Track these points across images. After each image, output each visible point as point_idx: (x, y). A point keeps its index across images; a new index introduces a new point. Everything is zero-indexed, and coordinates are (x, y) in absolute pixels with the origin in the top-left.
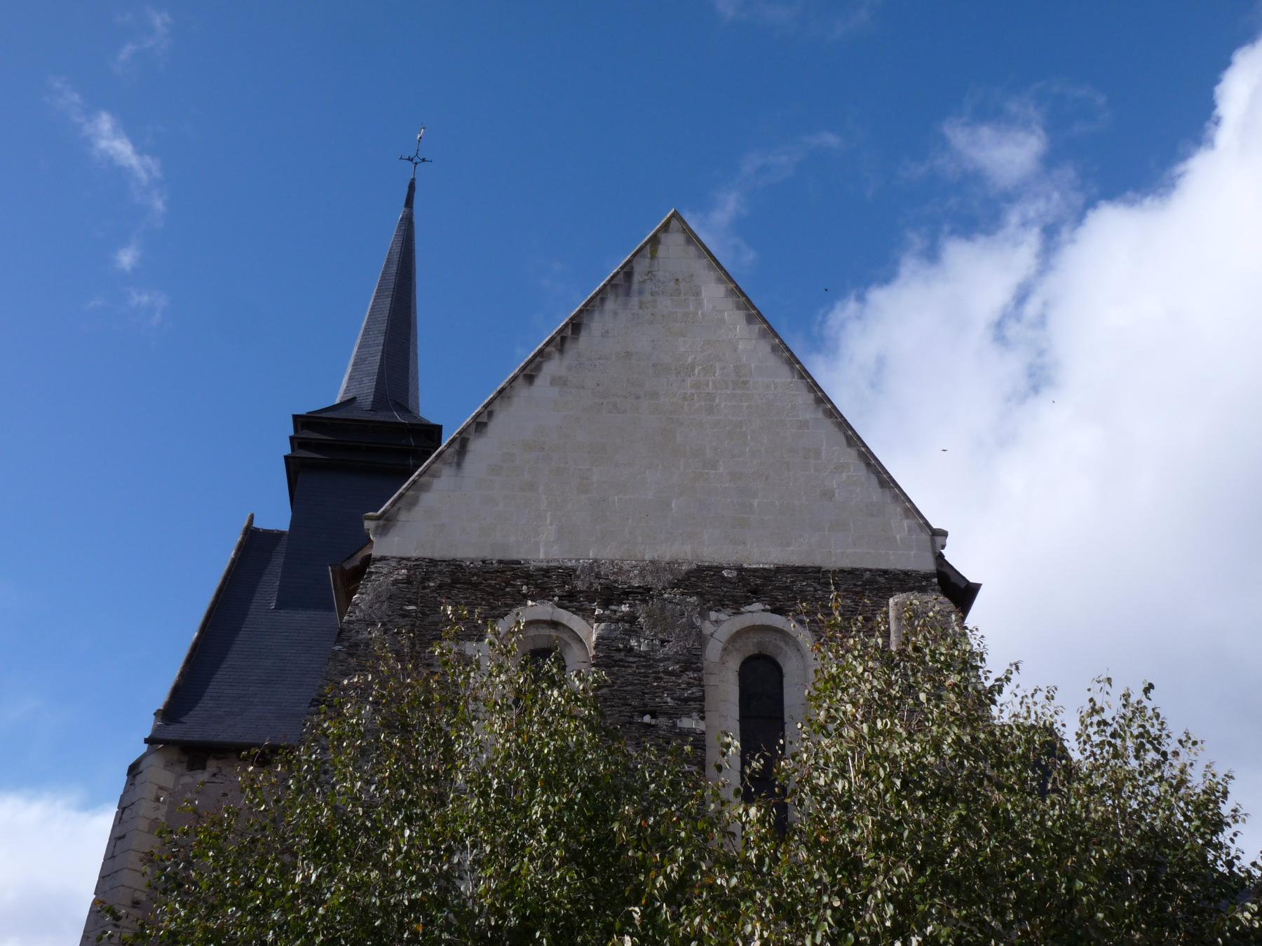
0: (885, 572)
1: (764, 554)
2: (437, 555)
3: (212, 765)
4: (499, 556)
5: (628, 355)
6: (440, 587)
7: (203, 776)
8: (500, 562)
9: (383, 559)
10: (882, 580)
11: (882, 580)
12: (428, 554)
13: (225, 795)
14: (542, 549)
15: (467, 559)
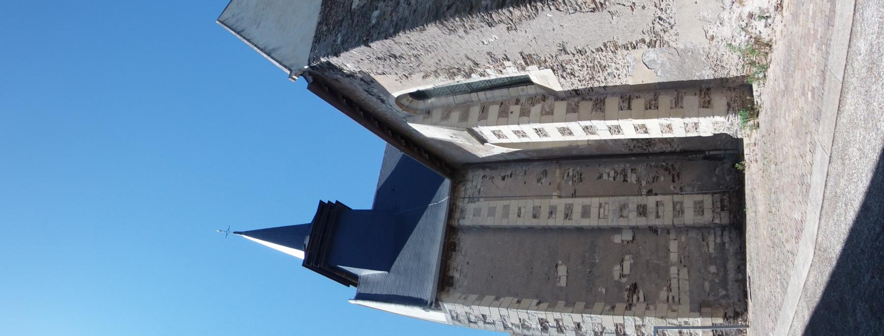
13: (468, 263)
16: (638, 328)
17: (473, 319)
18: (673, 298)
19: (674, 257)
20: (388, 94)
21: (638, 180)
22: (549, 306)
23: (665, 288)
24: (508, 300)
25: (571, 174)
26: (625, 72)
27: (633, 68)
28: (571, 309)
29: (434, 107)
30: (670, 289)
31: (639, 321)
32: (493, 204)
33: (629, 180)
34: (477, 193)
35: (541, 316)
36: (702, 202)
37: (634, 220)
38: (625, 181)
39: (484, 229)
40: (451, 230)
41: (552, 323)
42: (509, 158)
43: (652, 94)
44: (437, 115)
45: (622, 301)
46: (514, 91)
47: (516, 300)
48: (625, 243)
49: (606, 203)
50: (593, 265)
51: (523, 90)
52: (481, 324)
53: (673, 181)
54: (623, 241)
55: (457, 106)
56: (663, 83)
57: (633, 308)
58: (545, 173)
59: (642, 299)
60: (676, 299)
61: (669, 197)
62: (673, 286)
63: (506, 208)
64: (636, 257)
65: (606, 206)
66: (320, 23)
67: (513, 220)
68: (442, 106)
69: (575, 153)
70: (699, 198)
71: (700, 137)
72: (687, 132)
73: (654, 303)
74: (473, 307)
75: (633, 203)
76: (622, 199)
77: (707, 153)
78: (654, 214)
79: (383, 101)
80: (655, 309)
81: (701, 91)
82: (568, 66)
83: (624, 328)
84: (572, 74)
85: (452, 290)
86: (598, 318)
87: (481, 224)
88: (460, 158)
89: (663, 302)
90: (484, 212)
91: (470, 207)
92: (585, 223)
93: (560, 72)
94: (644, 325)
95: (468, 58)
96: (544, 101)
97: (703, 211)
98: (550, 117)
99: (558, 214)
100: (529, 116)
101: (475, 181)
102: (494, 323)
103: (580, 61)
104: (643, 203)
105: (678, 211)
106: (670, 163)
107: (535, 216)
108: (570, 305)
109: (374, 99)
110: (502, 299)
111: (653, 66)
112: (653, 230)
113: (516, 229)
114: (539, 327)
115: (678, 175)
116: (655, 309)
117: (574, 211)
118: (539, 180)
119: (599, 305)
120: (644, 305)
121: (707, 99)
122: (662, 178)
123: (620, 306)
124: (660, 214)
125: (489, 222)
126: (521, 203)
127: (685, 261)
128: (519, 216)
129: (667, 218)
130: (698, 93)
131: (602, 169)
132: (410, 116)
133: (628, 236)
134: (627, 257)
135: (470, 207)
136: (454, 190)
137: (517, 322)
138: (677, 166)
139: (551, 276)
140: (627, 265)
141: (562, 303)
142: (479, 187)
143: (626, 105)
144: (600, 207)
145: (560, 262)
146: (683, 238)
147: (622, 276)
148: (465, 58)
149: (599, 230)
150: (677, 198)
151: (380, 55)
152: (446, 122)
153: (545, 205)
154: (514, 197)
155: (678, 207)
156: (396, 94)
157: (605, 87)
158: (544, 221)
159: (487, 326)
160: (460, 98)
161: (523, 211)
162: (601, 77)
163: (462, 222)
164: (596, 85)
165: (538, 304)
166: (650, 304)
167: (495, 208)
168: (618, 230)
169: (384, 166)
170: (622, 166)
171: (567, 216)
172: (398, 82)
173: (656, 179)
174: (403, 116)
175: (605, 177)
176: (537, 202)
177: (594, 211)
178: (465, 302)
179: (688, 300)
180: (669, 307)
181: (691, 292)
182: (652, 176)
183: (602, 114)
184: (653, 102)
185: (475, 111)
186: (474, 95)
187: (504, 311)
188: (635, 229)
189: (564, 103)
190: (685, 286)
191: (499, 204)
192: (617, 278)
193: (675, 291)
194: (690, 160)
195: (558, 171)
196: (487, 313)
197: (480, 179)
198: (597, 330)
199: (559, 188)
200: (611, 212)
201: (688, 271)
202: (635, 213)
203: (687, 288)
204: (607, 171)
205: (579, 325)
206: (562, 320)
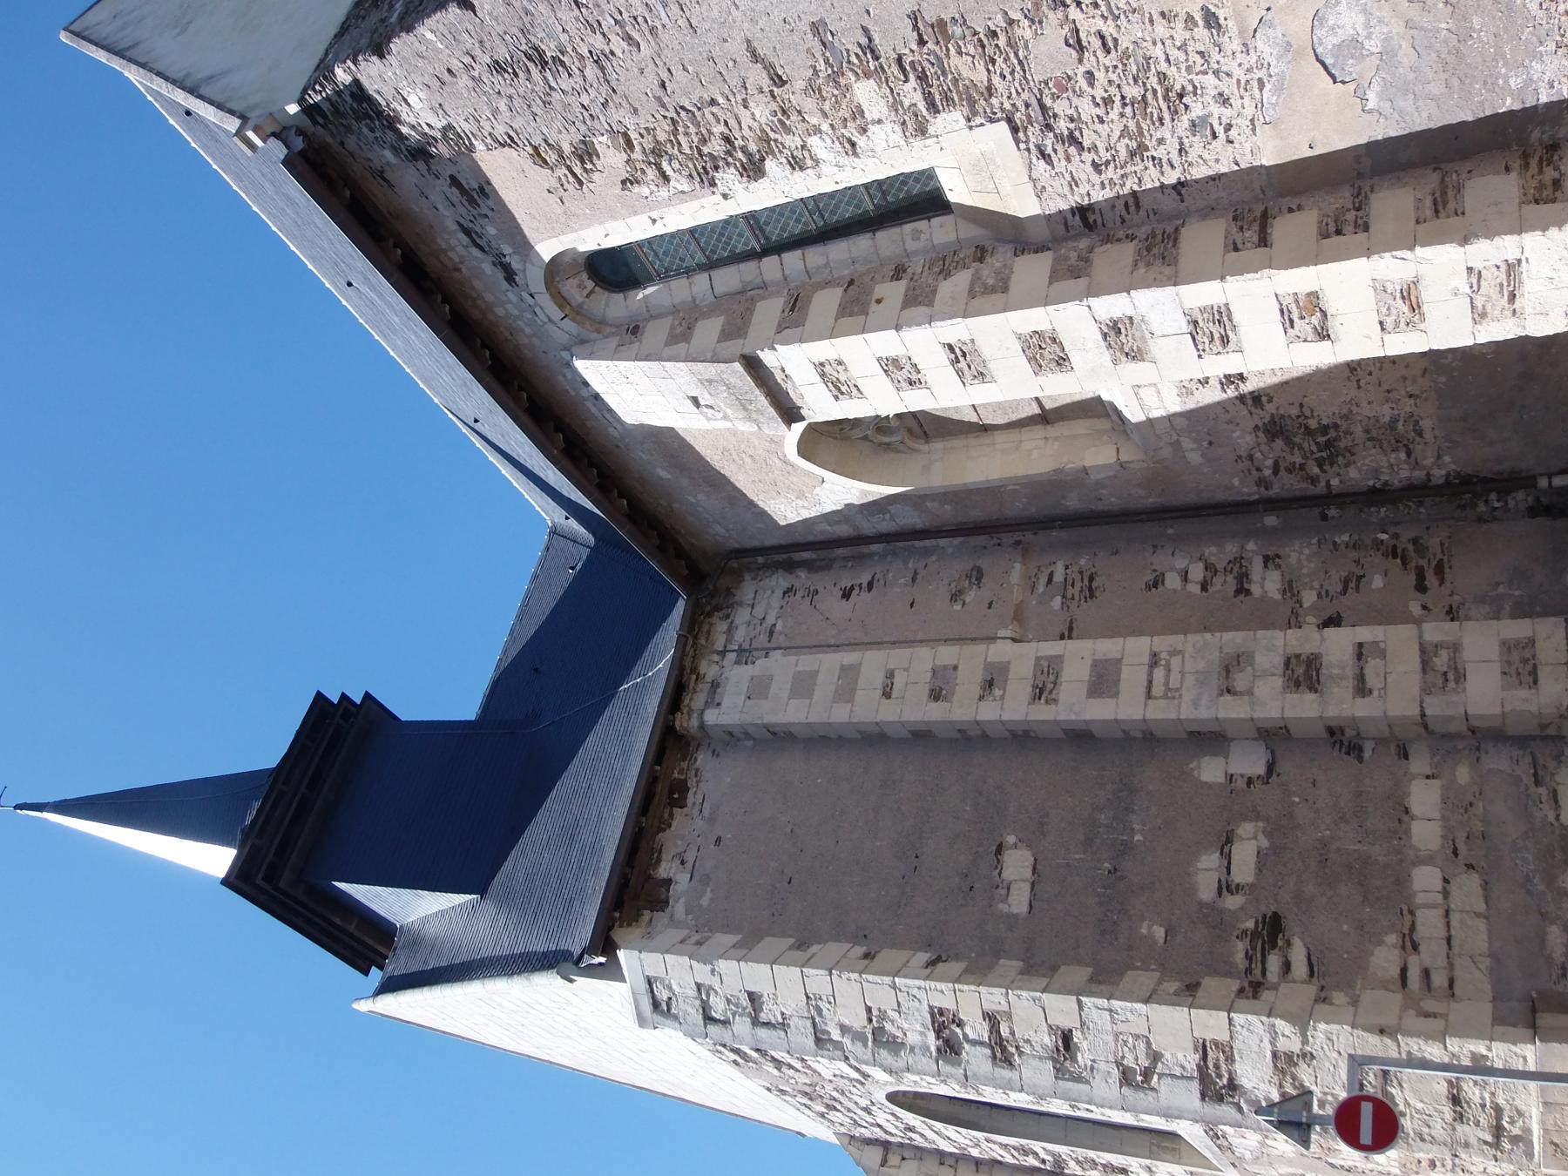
7: (682, 881)
17: (718, 1008)
18: (1426, 973)
19: (1426, 833)
20: (525, 248)
21: (1290, 589)
22: (966, 971)
23: (1392, 939)
25: (1059, 577)
26: (1250, 111)
27: (1279, 89)
29: (652, 313)
30: (1410, 943)
31: (1290, 1040)
32: (807, 662)
33: (1256, 590)
34: (764, 637)
35: (939, 1001)
36: (1531, 642)
37: (1271, 701)
38: (1242, 591)
39: (779, 738)
40: (671, 743)
41: (976, 1028)
42: (869, 527)
43: (1347, 193)
44: (656, 333)
46: (889, 241)
48: (1241, 784)
49: (1173, 653)
50: (1124, 850)
51: (916, 235)
52: (742, 1025)
53: (1421, 587)
55: (720, 303)
56: (1389, 142)
57: (1267, 995)
58: (977, 576)
59: (1300, 968)
60: (1439, 980)
61: (1405, 631)
62: (1422, 931)
64: (1279, 829)
65: (1176, 663)
67: (868, 709)
68: (675, 310)
69: (1073, 502)
70: (1519, 629)
71: (1525, 341)
72: (1480, 316)
74: (724, 965)
76: (1233, 639)
77: (1543, 483)
78: (1350, 683)
79: (510, 275)
80: (1355, 1002)
81: (1525, 156)
82: (1061, 107)
83: (1230, 1059)
84: (1073, 140)
85: (661, 918)
86: (1134, 1014)
87: (769, 719)
88: (720, 530)
90: (781, 686)
91: (737, 677)
92: (1099, 711)
93: (1034, 133)
94: (1308, 1057)
95: (755, 56)
96: (981, 260)
97: (1534, 673)
98: (998, 298)
100: (931, 304)
101: (762, 603)
102: (784, 1026)
103: (1100, 76)
104: (1308, 648)
105: (1441, 670)
106: (1407, 533)
107: (936, 695)
108: (1039, 968)
109: (487, 267)
110: (815, 948)
111: (1352, 68)
112: (1342, 740)
113: (873, 739)
114: (932, 1041)
115: (1439, 570)
117: (1065, 676)
118: (955, 597)
120: (1312, 990)
121: (1550, 174)
122: (1378, 581)
124: (1372, 681)
125: (794, 713)
126: (896, 658)
128: (887, 695)
129: (1399, 694)
130: (1517, 164)
131: (1160, 560)
132: (583, 342)
133: (1249, 761)
134: (1246, 829)
135: (737, 677)
136: (693, 628)
137: (858, 1021)
138: (1433, 543)
139: (979, 877)
140: (1245, 856)
142: (770, 620)
143: (1252, 235)
146: (1463, 774)
147: (1226, 887)
148: (744, 58)
149: (1143, 741)
151: (502, 54)
152: (682, 347)
153: (970, 662)
154: (878, 644)
155: (1441, 661)
156: (547, 250)
157: (1180, 185)
158: (964, 708)
159: (763, 1033)
160: (728, 279)
161: (899, 681)
162: (1167, 138)
163: (711, 717)
164: (1152, 179)
165: (931, 964)
166: (1331, 984)
168: (1211, 739)
169: (520, 617)
170: (1232, 549)
171: (1041, 693)
172: (554, 199)
173: (1354, 582)
174: (562, 338)
175: (1172, 581)
176: (947, 654)
177: (1132, 678)
178: (697, 943)
179: (1488, 987)
181: (1494, 955)
182: (1337, 576)
184: (1351, 215)
185: (770, 310)
186: (770, 262)
187: (818, 980)
189: (1045, 261)
190: (1475, 937)
191: (829, 664)
192: (1206, 887)
193: (1431, 953)
194: (1481, 520)
195: (1017, 566)
196: (764, 989)
197: (776, 600)
198: (1129, 1061)
199: (1019, 616)
200: (1190, 680)
201: (1485, 885)
202: (1278, 682)
203: (1481, 944)
204: (1180, 563)
205: (1067, 1038)
206: (1009, 1015)
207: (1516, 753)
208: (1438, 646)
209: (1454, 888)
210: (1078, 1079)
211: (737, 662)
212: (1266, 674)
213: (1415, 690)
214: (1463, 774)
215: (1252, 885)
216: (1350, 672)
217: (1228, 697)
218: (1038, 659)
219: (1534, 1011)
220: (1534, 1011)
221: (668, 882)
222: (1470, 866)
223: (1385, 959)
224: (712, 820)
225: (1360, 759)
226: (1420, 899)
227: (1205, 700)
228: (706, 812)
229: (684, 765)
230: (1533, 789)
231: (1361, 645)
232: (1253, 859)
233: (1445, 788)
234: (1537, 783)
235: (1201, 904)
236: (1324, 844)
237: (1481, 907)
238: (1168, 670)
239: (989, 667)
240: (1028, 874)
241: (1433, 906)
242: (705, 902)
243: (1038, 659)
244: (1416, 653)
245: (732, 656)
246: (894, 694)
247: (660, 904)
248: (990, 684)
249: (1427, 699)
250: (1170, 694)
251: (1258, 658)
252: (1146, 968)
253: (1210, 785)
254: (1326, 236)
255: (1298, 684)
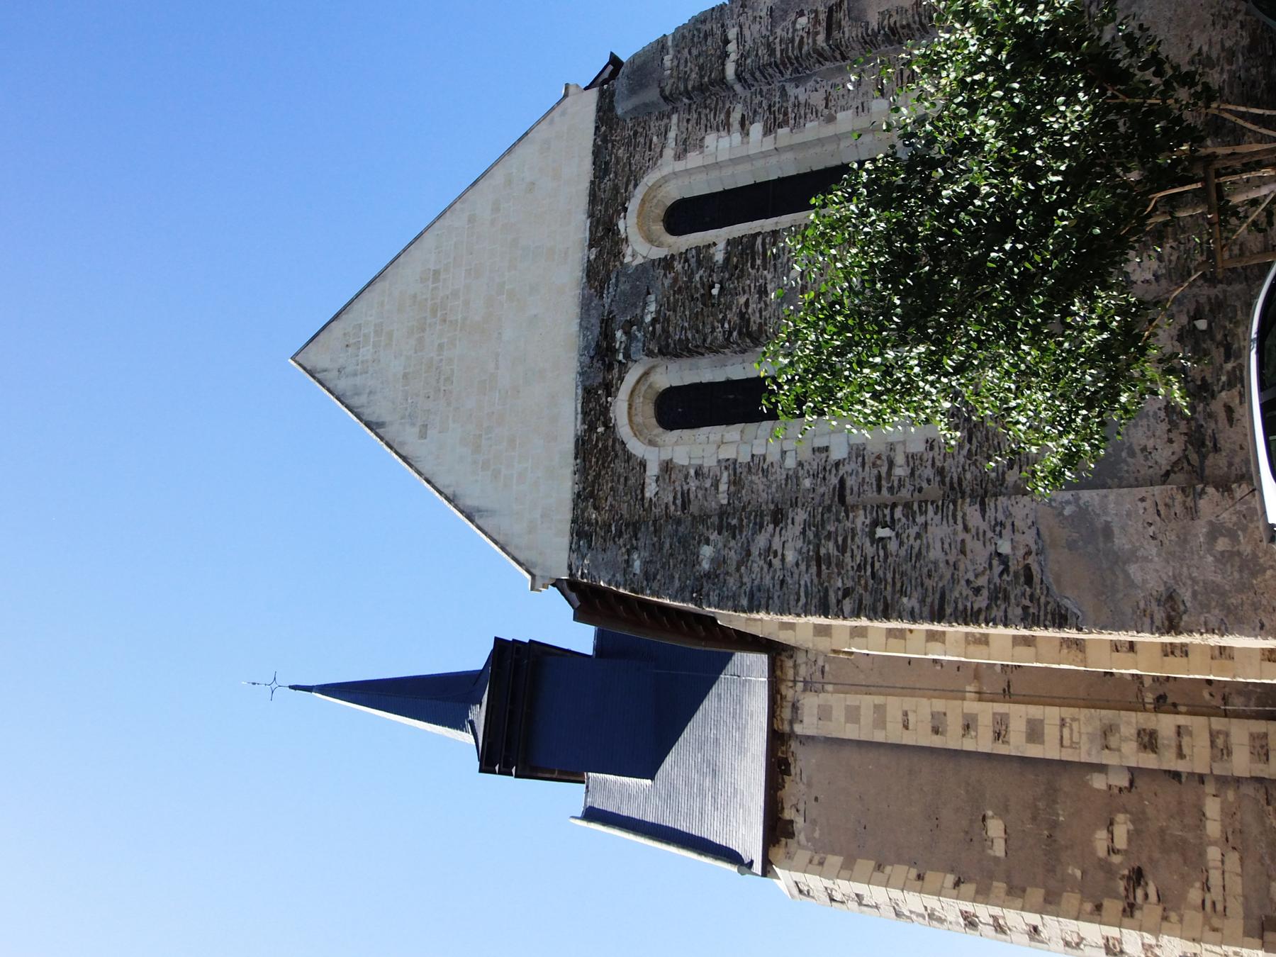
0: (597, 128)
1: (578, 227)
2: (569, 516)
3: (788, 814)
4: (571, 460)
5: (405, 376)
6: (596, 508)
7: (799, 823)
8: (576, 458)
9: (570, 567)
10: (603, 129)
11: (603, 129)
12: (567, 527)
13: (816, 799)
14: (567, 421)
15: (573, 488)
16: (1147, 948)
17: (838, 896)
18: (1214, 904)
19: (1213, 828)
23: (1198, 885)
24: (900, 871)
28: (1019, 902)
30: (1206, 887)
31: (1149, 939)
34: (818, 674)
36: (1266, 735)
40: (778, 740)
45: (1116, 896)
47: (914, 872)
48: (1116, 791)
49: (1074, 719)
50: (1054, 825)
54: (1110, 787)
57: (1138, 914)
60: (1219, 907)
62: (1212, 882)
63: (880, 710)
64: (1139, 819)
65: (1075, 725)
66: (579, 498)
73: (1176, 908)
74: (839, 881)
75: (1129, 723)
78: (1174, 750)
80: (1181, 921)
89: (1195, 908)
91: (810, 703)
92: (1034, 751)
97: (1267, 755)
99: (980, 730)
105: (1222, 750)
110: (888, 869)
116: (1181, 921)
117: (1012, 727)
119: (1071, 899)
120: (1159, 909)
123: (1113, 906)
124: (1186, 750)
127: (1234, 839)
128: (906, 727)
129: (1199, 759)
134: (1120, 817)
139: (974, 835)
141: (1000, 887)
144: (1063, 724)
145: (990, 813)
146: (1231, 795)
147: (1112, 850)
150: (1218, 723)
155: (1220, 742)
158: (953, 740)
161: (912, 717)
165: (957, 884)
167: (858, 708)
168: (1102, 768)
176: (939, 705)
177: (1051, 732)
179: (1240, 910)
180: (1207, 921)
183: (1080, 655)
187: (896, 893)
188: (1134, 772)
192: (1101, 851)
193: (1216, 894)
198: (1069, 939)
200: (1084, 738)
201: (1241, 859)
202: (1134, 745)
203: (1239, 890)
207: (1258, 785)
208: (1219, 732)
209: (1226, 860)
210: (1042, 942)
211: (805, 690)
212: (1126, 739)
213: (1208, 759)
214: (1231, 795)
215: (1126, 851)
216: (1174, 744)
217: (1106, 751)
218: (994, 714)
219: (1263, 930)
220: (1263, 930)
221: (791, 822)
222: (1234, 848)
223: (1195, 895)
224: (809, 785)
225: (1180, 782)
226: (1211, 864)
227: (1094, 752)
228: (805, 779)
229: (784, 748)
230: (1266, 807)
231: (1179, 727)
232: (1125, 836)
233: (1222, 803)
234: (1268, 803)
235: (1100, 859)
236: (1162, 831)
237: (1239, 870)
238: (1071, 730)
239: (965, 716)
240: (1002, 834)
241: (1216, 868)
242: (817, 835)
243: (994, 714)
244: (1207, 735)
245: (800, 686)
246: (911, 727)
247: (791, 835)
248: (967, 727)
249: (1215, 765)
250: (1074, 746)
251: (1123, 729)
252: (1073, 891)
253: (1098, 790)
254: (1166, 655)
255: (1145, 747)
